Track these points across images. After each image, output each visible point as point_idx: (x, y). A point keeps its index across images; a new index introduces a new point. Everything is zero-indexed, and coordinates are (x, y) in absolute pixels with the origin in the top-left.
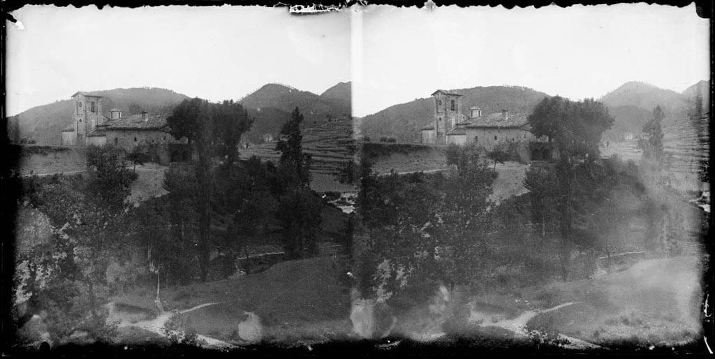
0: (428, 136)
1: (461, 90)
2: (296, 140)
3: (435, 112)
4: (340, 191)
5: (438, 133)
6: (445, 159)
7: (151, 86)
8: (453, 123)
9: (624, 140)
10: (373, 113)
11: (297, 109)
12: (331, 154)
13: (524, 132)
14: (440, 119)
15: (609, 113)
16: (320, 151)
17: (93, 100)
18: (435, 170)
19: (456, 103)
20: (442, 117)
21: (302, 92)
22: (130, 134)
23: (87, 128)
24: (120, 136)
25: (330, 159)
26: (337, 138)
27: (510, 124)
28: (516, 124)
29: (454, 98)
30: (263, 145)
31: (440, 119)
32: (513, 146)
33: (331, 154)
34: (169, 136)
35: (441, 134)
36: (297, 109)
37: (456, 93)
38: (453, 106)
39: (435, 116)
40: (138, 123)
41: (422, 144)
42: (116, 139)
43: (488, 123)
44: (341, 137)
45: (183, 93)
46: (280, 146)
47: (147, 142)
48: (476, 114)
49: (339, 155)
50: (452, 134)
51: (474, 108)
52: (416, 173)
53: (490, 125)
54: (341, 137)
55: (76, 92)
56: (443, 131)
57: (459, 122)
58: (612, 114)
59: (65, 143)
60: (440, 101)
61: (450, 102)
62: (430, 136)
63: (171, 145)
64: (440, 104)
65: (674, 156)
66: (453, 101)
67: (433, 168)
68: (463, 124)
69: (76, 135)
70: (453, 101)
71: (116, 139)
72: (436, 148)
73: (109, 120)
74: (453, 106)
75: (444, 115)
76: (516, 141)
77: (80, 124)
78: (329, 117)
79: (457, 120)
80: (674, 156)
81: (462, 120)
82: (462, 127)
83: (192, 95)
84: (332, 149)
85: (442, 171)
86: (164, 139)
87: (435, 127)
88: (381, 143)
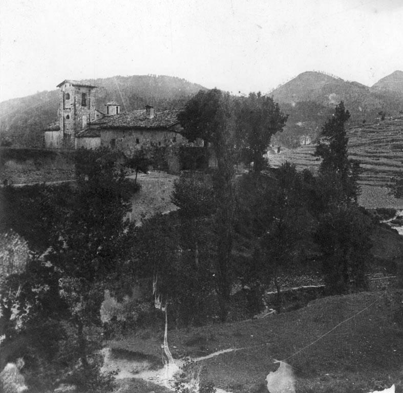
9: (300, 146)
11: (260, 93)
13: (174, 134)
14: (68, 117)
16: (370, 157)
19: (87, 97)
21: (348, 82)
23: (76, 126)
24: (120, 138)
26: (393, 141)
27: (154, 124)
30: (299, 150)
31: (68, 117)
34: (179, 137)
36: (260, 93)
40: (141, 120)
46: (320, 151)
47: (152, 144)
50: (83, 136)
57: (91, 121)
64: (68, 98)
69: (62, 135)
70: (84, 95)
73: (104, 116)
75: (73, 111)
76: (162, 145)
77: (66, 122)
78: (382, 115)
84: (385, 154)
86: (174, 140)
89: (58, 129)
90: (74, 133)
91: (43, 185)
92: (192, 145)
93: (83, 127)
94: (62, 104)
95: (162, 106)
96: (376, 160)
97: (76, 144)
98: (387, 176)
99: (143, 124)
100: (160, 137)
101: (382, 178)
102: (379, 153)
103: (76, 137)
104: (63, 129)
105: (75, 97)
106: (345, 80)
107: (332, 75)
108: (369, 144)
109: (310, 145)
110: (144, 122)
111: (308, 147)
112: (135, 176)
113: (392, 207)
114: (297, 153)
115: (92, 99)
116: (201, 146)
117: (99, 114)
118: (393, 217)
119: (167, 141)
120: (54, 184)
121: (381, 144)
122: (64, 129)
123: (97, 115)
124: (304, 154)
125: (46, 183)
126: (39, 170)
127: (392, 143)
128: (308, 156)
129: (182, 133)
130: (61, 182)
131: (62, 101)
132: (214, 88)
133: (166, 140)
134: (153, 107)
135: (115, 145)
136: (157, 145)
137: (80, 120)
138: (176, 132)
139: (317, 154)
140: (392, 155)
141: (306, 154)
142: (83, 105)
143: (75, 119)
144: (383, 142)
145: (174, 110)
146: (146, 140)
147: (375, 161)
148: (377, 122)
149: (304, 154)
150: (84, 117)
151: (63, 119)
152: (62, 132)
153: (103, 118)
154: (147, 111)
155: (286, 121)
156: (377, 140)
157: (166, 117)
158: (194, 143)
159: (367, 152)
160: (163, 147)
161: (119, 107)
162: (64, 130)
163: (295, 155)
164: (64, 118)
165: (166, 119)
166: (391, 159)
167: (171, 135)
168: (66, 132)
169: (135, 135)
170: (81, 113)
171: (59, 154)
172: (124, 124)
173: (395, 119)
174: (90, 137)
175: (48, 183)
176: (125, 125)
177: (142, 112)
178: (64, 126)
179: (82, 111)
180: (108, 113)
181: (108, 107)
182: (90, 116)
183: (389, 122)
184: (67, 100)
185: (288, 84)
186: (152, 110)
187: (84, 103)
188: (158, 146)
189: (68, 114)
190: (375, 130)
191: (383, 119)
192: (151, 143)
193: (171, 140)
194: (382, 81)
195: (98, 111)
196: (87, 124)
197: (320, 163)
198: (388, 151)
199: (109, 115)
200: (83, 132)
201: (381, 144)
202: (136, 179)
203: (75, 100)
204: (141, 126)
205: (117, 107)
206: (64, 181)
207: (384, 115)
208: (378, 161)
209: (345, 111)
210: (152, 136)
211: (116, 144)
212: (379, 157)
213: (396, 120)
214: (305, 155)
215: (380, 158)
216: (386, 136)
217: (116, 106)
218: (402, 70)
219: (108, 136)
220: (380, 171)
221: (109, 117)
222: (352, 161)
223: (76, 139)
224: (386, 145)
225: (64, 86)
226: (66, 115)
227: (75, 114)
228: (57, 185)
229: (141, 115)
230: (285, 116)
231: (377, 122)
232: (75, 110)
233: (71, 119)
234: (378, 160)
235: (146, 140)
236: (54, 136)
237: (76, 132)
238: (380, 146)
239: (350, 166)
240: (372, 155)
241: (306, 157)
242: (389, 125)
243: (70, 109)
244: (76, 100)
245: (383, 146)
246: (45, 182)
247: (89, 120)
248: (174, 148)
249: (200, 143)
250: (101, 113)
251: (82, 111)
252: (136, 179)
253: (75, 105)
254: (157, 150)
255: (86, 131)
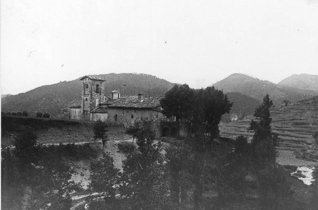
0: (76, 112)
1: (104, 75)
2: (267, 121)
3: (83, 93)
4: (297, 165)
5: (84, 111)
6: (92, 133)
7: (138, 72)
8: (97, 104)
9: (230, 121)
10: (24, 92)
11: (267, 96)
12: (288, 133)
13: (157, 112)
14: (86, 99)
15: (228, 100)
16: (278, 130)
17: (98, 83)
18: (84, 143)
19: (100, 87)
20: (88, 98)
21: (262, 81)
22: (128, 112)
23: (92, 105)
24: (120, 113)
25: (288, 138)
26: (293, 120)
27: (144, 106)
28: (150, 106)
29: (98, 83)
30: (230, 124)
31: (86, 99)
32: (147, 124)
33: (288, 133)
34: (160, 115)
35: (87, 111)
36: (267, 96)
37: (100, 79)
38: (97, 89)
39: (82, 97)
40: (135, 103)
41: (70, 120)
42: (116, 116)
43: (126, 104)
44: (296, 120)
45: (79, 77)
46: (253, 125)
47: (142, 119)
48: (116, 96)
49: (295, 135)
50: (96, 112)
51: (115, 91)
52: (69, 145)
53: (128, 105)
54: (296, 120)
55: (84, 76)
56: (89, 109)
57: (101, 103)
58: (230, 100)
59: (72, 118)
60: (87, 85)
61: (95, 87)
62: (77, 113)
63: (163, 123)
64: (87, 88)
65: (279, 137)
66: (97, 86)
67: (82, 141)
68: (105, 105)
69: (82, 111)
70: (97, 86)
71: (116, 116)
72: (84, 124)
73: (110, 99)
74: (97, 89)
75: (89, 96)
76: (149, 119)
77: (86, 102)
78: (286, 102)
79: (100, 101)
80: (279, 137)
81: (104, 101)
82: (105, 106)
83: (181, 82)
84: (288, 129)
85: (90, 143)
86: (157, 117)
87: (82, 105)
88: (37, 118)
89: (79, 107)
90: (90, 110)
91: (73, 145)
92: (168, 120)
93: (96, 106)
94: (83, 91)
95: (150, 93)
96: (282, 132)
97: (91, 117)
98: (289, 144)
99: (136, 106)
100: (147, 115)
101: (286, 144)
102: (284, 127)
103: (91, 113)
104: (83, 107)
105: (92, 87)
106: (260, 79)
107: (252, 76)
108: (278, 121)
109: (238, 121)
110: (137, 104)
111: (237, 122)
112: (132, 140)
113: (294, 165)
114: (229, 126)
115: (103, 88)
116: (174, 121)
117: (107, 98)
118: (295, 171)
119: (152, 117)
120: (80, 144)
121: (285, 122)
122: (83, 107)
123: (105, 99)
124: (234, 127)
125: (75, 143)
126: (70, 134)
127: (292, 121)
128: (236, 128)
129: (163, 112)
130: (84, 143)
131: (83, 89)
132: (184, 84)
133: (151, 117)
134: (142, 95)
135: (117, 119)
136: (145, 120)
137: (94, 101)
138: (158, 111)
139: (251, 128)
140: (293, 129)
141: (235, 127)
142: (96, 92)
143: (91, 101)
144: (287, 120)
145: (157, 97)
146: (138, 117)
147: (281, 133)
148: (282, 107)
149: (234, 127)
150: (97, 100)
151: (83, 101)
152: (82, 109)
153: (109, 101)
154: (139, 97)
155: (231, 106)
156: (283, 119)
157: (152, 101)
158: (169, 119)
159: (277, 127)
160: (149, 121)
161: (120, 94)
162: (83, 108)
163: (228, 127)
164: (84, 100)
165: (152, 102)
166: (292, 132)
167: (154, 114)
168: (85, 109)
169: (133, 113)
170: (95, 97)
171: (82, 124)
172: (124, 105)
173: (294, 105)
174: (101, 113)
175: (76, 144)
176: (124, 106)
177: (135, 98)
178: (84, 105)
179: (96, 96)
180: (112, 98)
181: (112, 94)
182: (100, 99)
183: (290, 107)
184: (86, 89)
185: (222, 81)
186: (142, 96)
187: (97, 91)
188: (146, 120)
189: (86, 98)
190: (281, 112)
191: (286, 105)
192: (141, 118)
193: (155, 117)
194: (283, 81)
195: (106, 96)
196: (99, 104)
197: (253, 134)
198: (290, 127)
199: (113, 99)
200: (96, 110)
201: (285, 122)
202: (133, 143)
203: (92, 89)
204: (135, 107)
205: (118, 94)
206: (86, 142)
207: (287, 103)
208: (284, 133)
209: (270, 101)
210: (142, 114)
211: (118, 118)
212: (284, 130)
213: (295, 106)
214: (234, 128)
215: (285, 131)
216: (289, 116)
217: (118, 94)
218: (317, 74)
219: (113, 112)
220: (285, 140)
221: (114, 100)
222: (273, 134)
223: (91, 114)
224: (289, 122)
225: (85, 80)
226: (85, 98)
227: (91, 98)
228: (81, 145)
229: (134, 100)
230: (231, 103)
231: (282, 107)
232: (92, 96)
233: (89, 101)
234: (284, 132)
235: (138, 117)
236: (77, 112)
237: (92, 110)
238: (285, 123)
239: (272, 137)
240: (279, 129)
241: (235, 129)
242: (290, 109)
243: (88, 94)
244: (93, 89)
245: (287, 123)
246: (74, 143)
247: (100, 101)
248: (156, 122)
249: (174, 119)
250: (108, 98)
251: (96, 96)
252: (133, 143)
253: (91, 92)
254: (145, 123)
255: (98, 108)
